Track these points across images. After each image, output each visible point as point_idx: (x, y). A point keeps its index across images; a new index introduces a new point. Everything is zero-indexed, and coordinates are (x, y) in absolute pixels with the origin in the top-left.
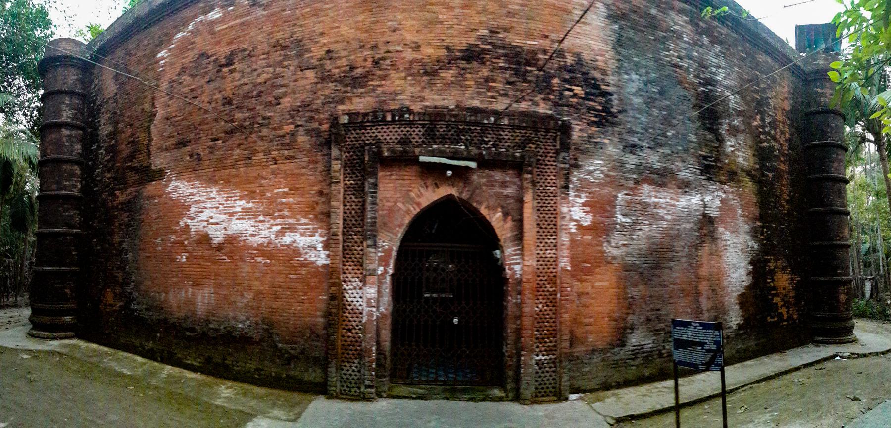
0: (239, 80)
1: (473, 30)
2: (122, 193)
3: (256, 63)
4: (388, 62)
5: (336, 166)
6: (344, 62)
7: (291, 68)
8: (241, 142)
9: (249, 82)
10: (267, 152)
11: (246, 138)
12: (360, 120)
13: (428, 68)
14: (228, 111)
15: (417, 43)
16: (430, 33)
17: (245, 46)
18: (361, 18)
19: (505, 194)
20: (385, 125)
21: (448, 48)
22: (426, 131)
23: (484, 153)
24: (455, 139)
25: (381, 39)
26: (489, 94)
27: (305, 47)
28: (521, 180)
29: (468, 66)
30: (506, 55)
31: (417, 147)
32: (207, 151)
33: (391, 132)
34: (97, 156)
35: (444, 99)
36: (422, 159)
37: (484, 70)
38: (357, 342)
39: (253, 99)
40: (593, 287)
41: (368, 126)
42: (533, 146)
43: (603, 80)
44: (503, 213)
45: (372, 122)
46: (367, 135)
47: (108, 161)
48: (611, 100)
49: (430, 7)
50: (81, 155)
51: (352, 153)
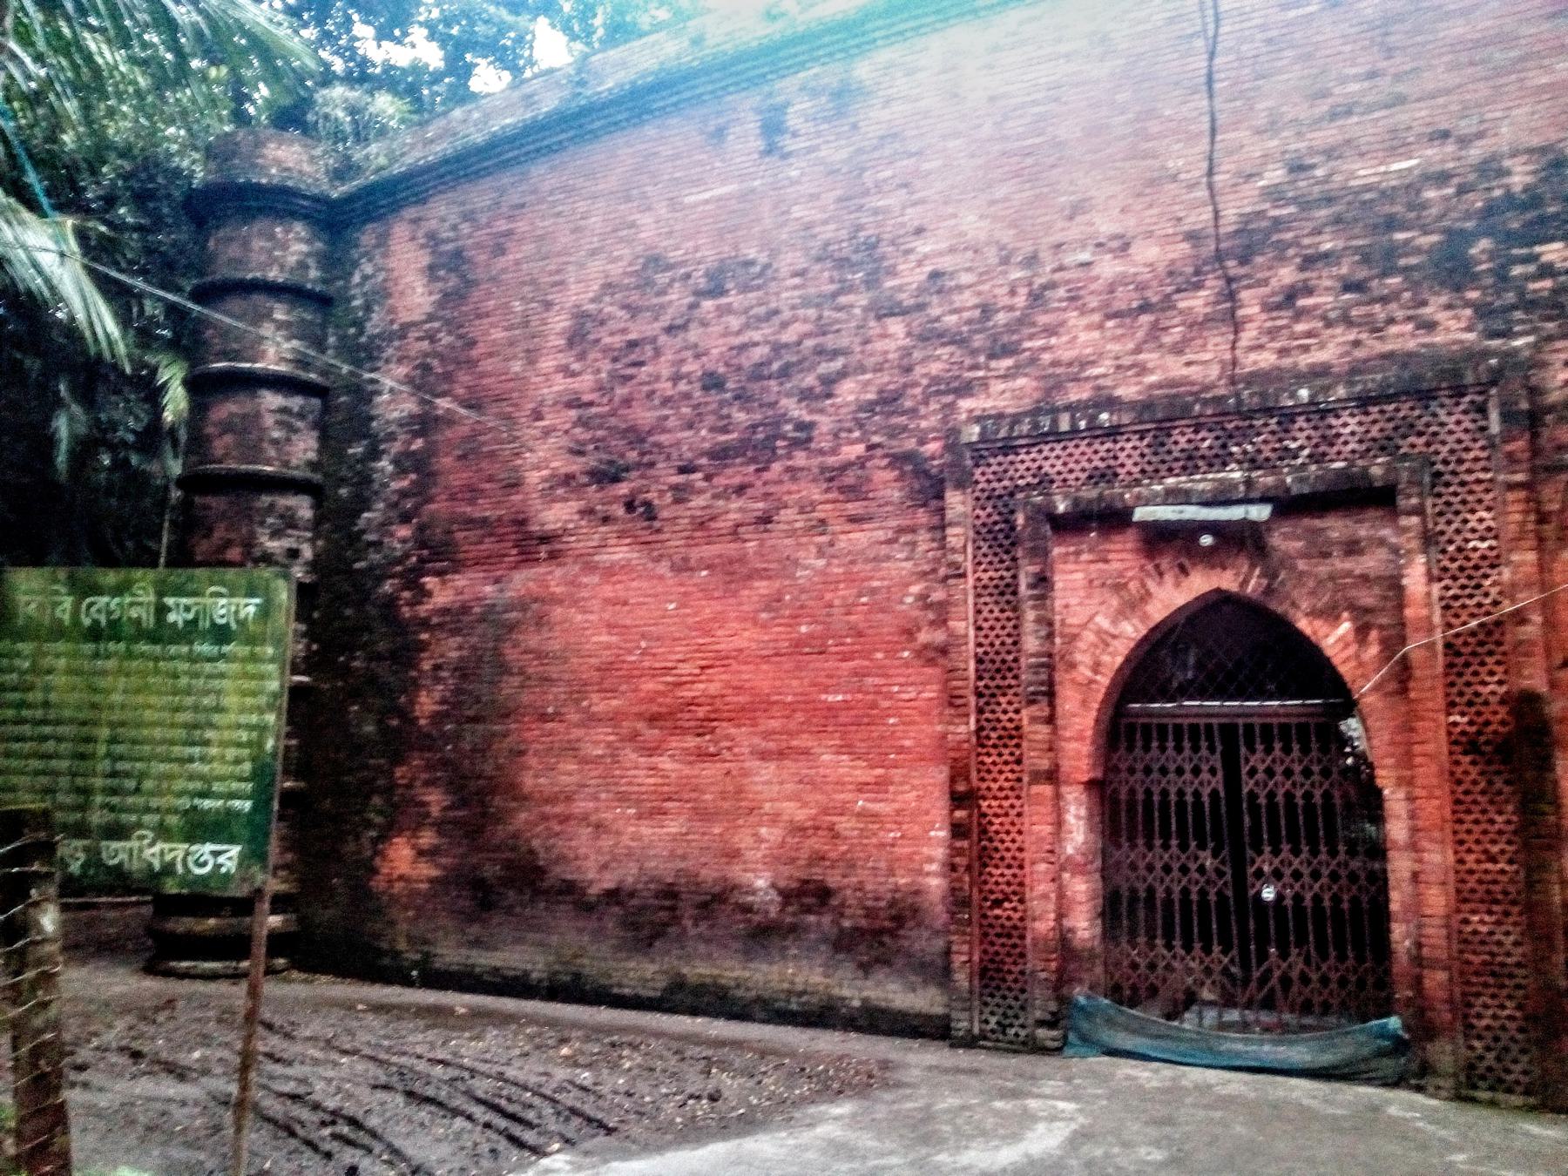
0: (739, 333)
2: (444, 583)
3: (777, 294)
4: (1061, 292)
6: (967, 299)
14: (714, 406)
15: (1122, 236)
19: (1357, 572)
20: (1059, 441)
23: (1289, 480)
26: (1300, 327)
27: (886, 264)
34: (365, 480)
36: (1141, 514)
41: (1022, 446)
47: (404, 494)
50: (313, 466)
51: (989, 510)
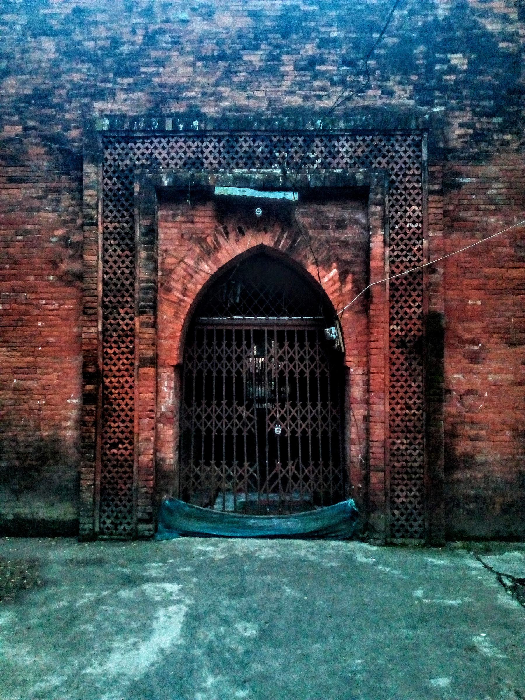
6: (101, 32)
12: (126, 126)
15: (209, 7)
19: (343, 239)
21: (252, 14)
24: (266, 158)
28: (367, 216)
30: (341, 19)
31: (210, 172)
36: (218, 190)
37: (308, 46)
38: (126, 460)
41: (139, 138)
45: (144, 131)
51: (115, 179)
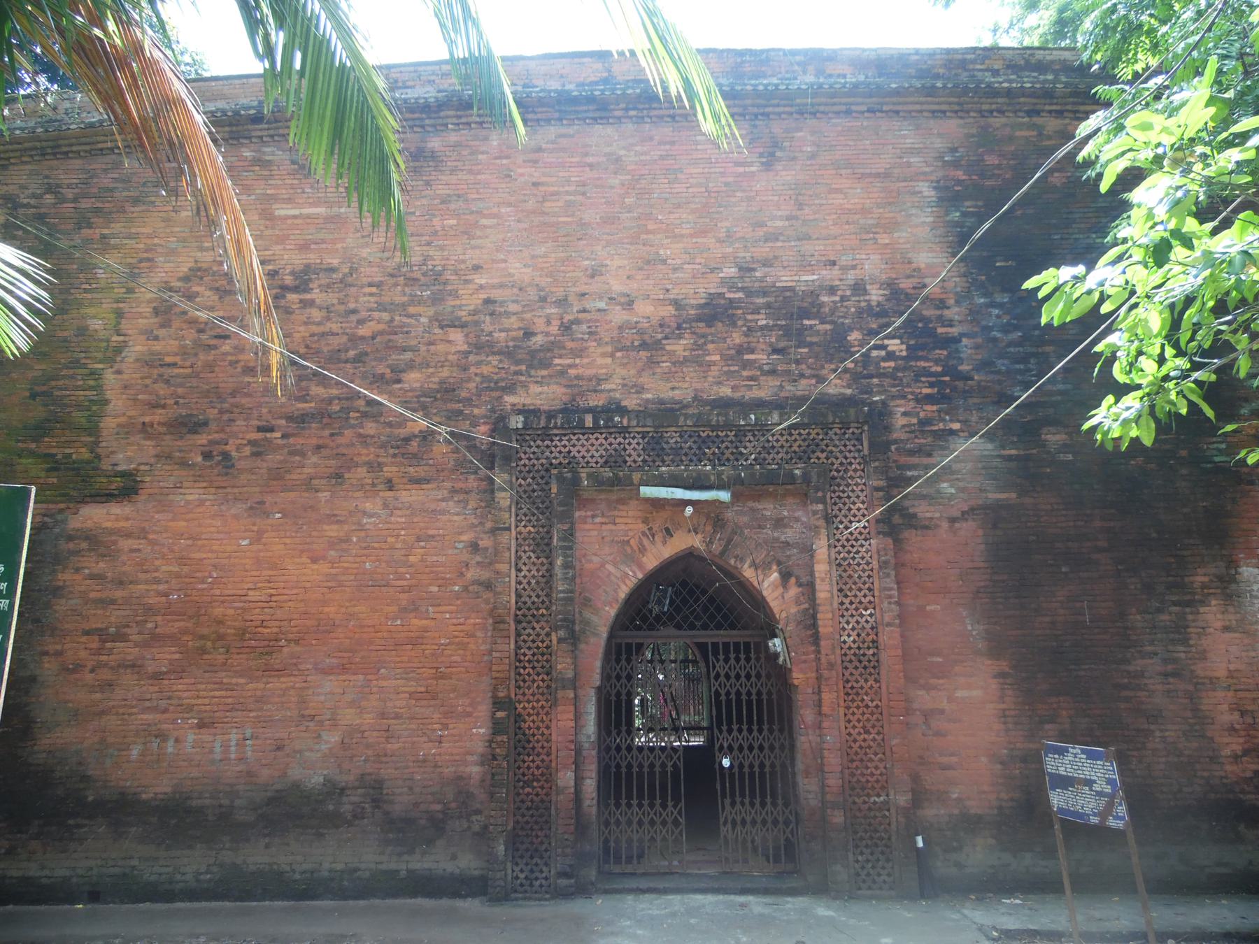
1: (712, 271)
4: (584, 327)
5: (504, 498)
7: (423, 320)
8: (321, 442)
9: (340, 331)
10: (375, 467)
11: (332, 435)
13: (646, 337)
16: (648, 278)
17: (335, 262)
18: (540, 250)
19: (783, 539)
21: (676, 304)
22: (648, 443)
24: (695, 454)
25: (574, 289)
26: (745, 373)
27: (449, 288)
29: (708, 331)
30: (768, 306)
32: (247, 451)
33: (593, 445)
35: (673, 389)
39: (348, 365)
40: (951, 699)
41: (556, 435)
42: (823, 456)
43: (940, 318)
44: (780, 573)
45: (562, 428)
46: (553, 449)
48: (957, 351)
49: (645, 236)
